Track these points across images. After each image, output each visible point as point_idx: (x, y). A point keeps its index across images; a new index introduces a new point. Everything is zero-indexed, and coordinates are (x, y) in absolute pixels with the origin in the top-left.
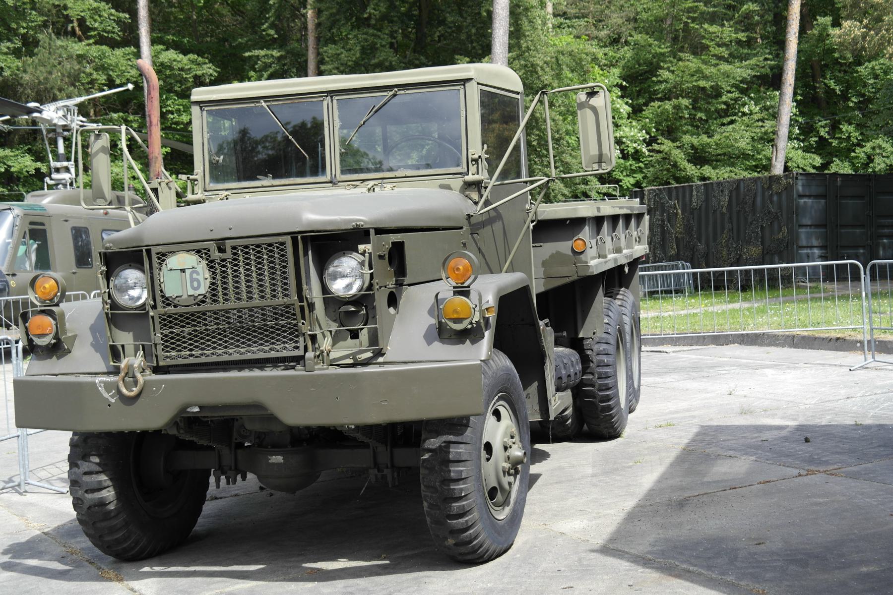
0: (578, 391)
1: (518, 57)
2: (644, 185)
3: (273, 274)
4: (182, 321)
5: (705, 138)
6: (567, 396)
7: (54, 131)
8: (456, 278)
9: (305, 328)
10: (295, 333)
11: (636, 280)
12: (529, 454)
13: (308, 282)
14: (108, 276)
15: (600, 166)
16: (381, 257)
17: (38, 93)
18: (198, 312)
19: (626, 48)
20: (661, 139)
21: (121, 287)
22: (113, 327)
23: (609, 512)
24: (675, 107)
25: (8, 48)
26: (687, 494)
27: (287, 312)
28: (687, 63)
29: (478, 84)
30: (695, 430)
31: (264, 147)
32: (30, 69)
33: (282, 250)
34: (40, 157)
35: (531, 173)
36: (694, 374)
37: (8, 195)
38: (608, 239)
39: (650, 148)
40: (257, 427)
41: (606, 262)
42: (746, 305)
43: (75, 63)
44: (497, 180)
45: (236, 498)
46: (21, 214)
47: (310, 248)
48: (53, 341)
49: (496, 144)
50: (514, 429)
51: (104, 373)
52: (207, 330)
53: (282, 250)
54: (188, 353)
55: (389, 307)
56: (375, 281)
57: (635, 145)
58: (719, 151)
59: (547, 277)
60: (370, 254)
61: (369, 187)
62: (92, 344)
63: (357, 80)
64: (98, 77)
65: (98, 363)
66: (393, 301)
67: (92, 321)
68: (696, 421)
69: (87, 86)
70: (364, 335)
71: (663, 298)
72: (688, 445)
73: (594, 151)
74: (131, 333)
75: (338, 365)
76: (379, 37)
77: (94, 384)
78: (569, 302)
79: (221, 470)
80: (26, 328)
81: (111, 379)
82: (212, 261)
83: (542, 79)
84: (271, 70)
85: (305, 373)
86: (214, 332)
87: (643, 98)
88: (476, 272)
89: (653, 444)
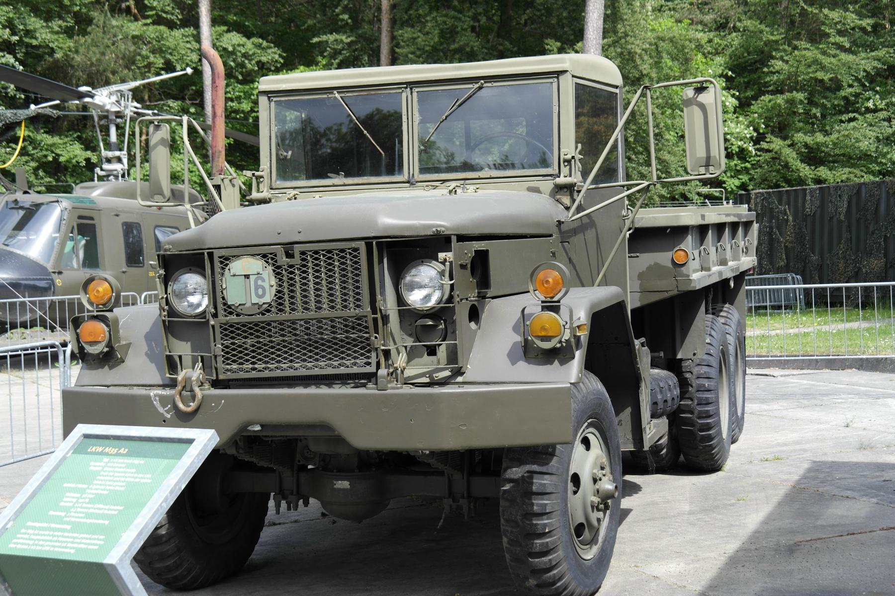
0: (675, 418)
1: (615, 43)
2: (751, 187)
3: (344, 282)
4: (245, 332)
5: (820, 138)
6: (664, 422)
7: (106, 117)
8: (545, 292)
9: (378, 343)
10: (367, 347)
11: (742, 295)
12: (620, 487)
13: (383, 293)
14: (166, 281)
15: (707, 170)
16: (463, 267)
17: (90, 76)
18: (263, 322)
19: (734, 34)
20: (769, 137)
21: (180, 292)
22: (170, 336)
23: (708, 554)
24: (787, 101)
25: (60, 27)
26: (799, 538)
27: (359, 325)
28: (804, 52)
29: (573, 76)
30: (806, 466)
31: (328, 140)
32: (82, 50)
33: (355, 257)
34: (89, 145)
35: (628, 177)
36: (805, 402)
37: (56, 186)
38: (712, 250)
39: (758, 146)
40: (322, 449)
41: (709, 276)
42: (865, 325)
43: (130, 43)
44: (593, 183)
45: (294, 525)
46: (69, 208)
47: (385, 254)
48: (106, 350)
49: (591, 142)
50: (605, 460)
51: (159, 386)
52: (271, 342)
53: (355, 257)
54: (251, 366)
55: (470, 321)
56: (456, 292)
57: (740, 143)
58: (837, 151)
59: (644, 291)
60: (451, 263)
61: (451, 188)
62: (146, 354)
63: (441, 70)
64: (155, 60)
65: (153, 374)
66: (474, 314)
67: (147, 329)
68: (808, 455)
69: (143, 70)
70: (442, 352)
71: (771, 315)
72: (798, 482)
73: (701, 153)
74: (189, 343)
75: (413, 384)
76: (460, 19)
77: (149, 397)
78: (666, 319)
79: (282, 494)
80: (77, 334)
81: (167, 392)
82: (279, 267)
83: (640, 68)
84: (341, 58)
85: (376, 392)
86: (279, 344)
87: (752, 90)
88: (567, 284)
89: (759, 480)
